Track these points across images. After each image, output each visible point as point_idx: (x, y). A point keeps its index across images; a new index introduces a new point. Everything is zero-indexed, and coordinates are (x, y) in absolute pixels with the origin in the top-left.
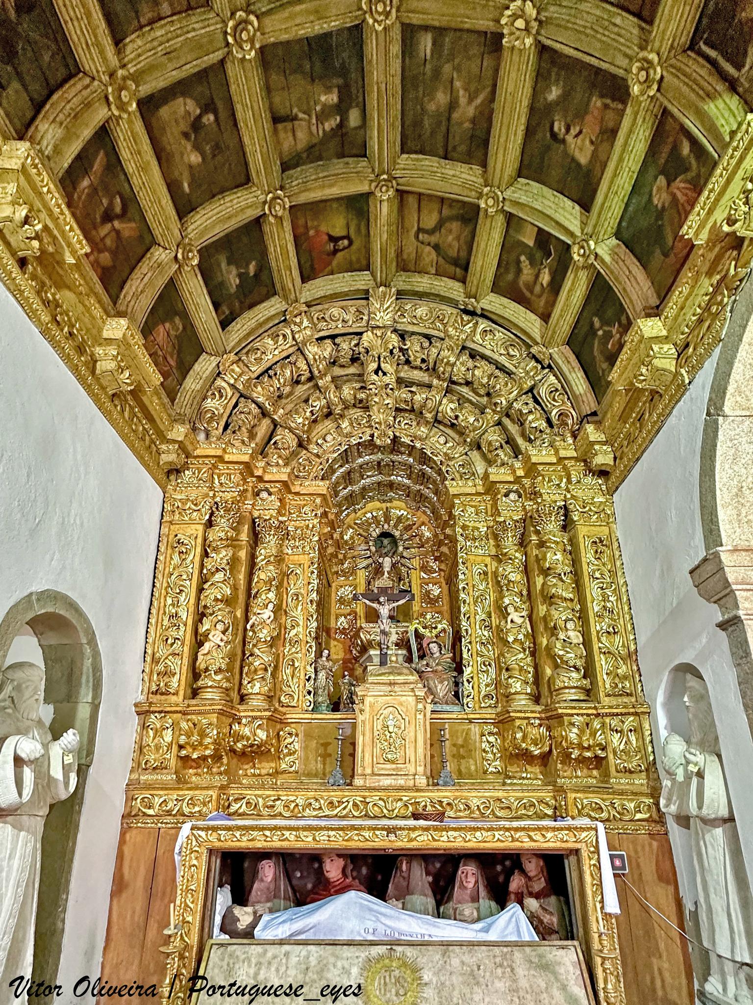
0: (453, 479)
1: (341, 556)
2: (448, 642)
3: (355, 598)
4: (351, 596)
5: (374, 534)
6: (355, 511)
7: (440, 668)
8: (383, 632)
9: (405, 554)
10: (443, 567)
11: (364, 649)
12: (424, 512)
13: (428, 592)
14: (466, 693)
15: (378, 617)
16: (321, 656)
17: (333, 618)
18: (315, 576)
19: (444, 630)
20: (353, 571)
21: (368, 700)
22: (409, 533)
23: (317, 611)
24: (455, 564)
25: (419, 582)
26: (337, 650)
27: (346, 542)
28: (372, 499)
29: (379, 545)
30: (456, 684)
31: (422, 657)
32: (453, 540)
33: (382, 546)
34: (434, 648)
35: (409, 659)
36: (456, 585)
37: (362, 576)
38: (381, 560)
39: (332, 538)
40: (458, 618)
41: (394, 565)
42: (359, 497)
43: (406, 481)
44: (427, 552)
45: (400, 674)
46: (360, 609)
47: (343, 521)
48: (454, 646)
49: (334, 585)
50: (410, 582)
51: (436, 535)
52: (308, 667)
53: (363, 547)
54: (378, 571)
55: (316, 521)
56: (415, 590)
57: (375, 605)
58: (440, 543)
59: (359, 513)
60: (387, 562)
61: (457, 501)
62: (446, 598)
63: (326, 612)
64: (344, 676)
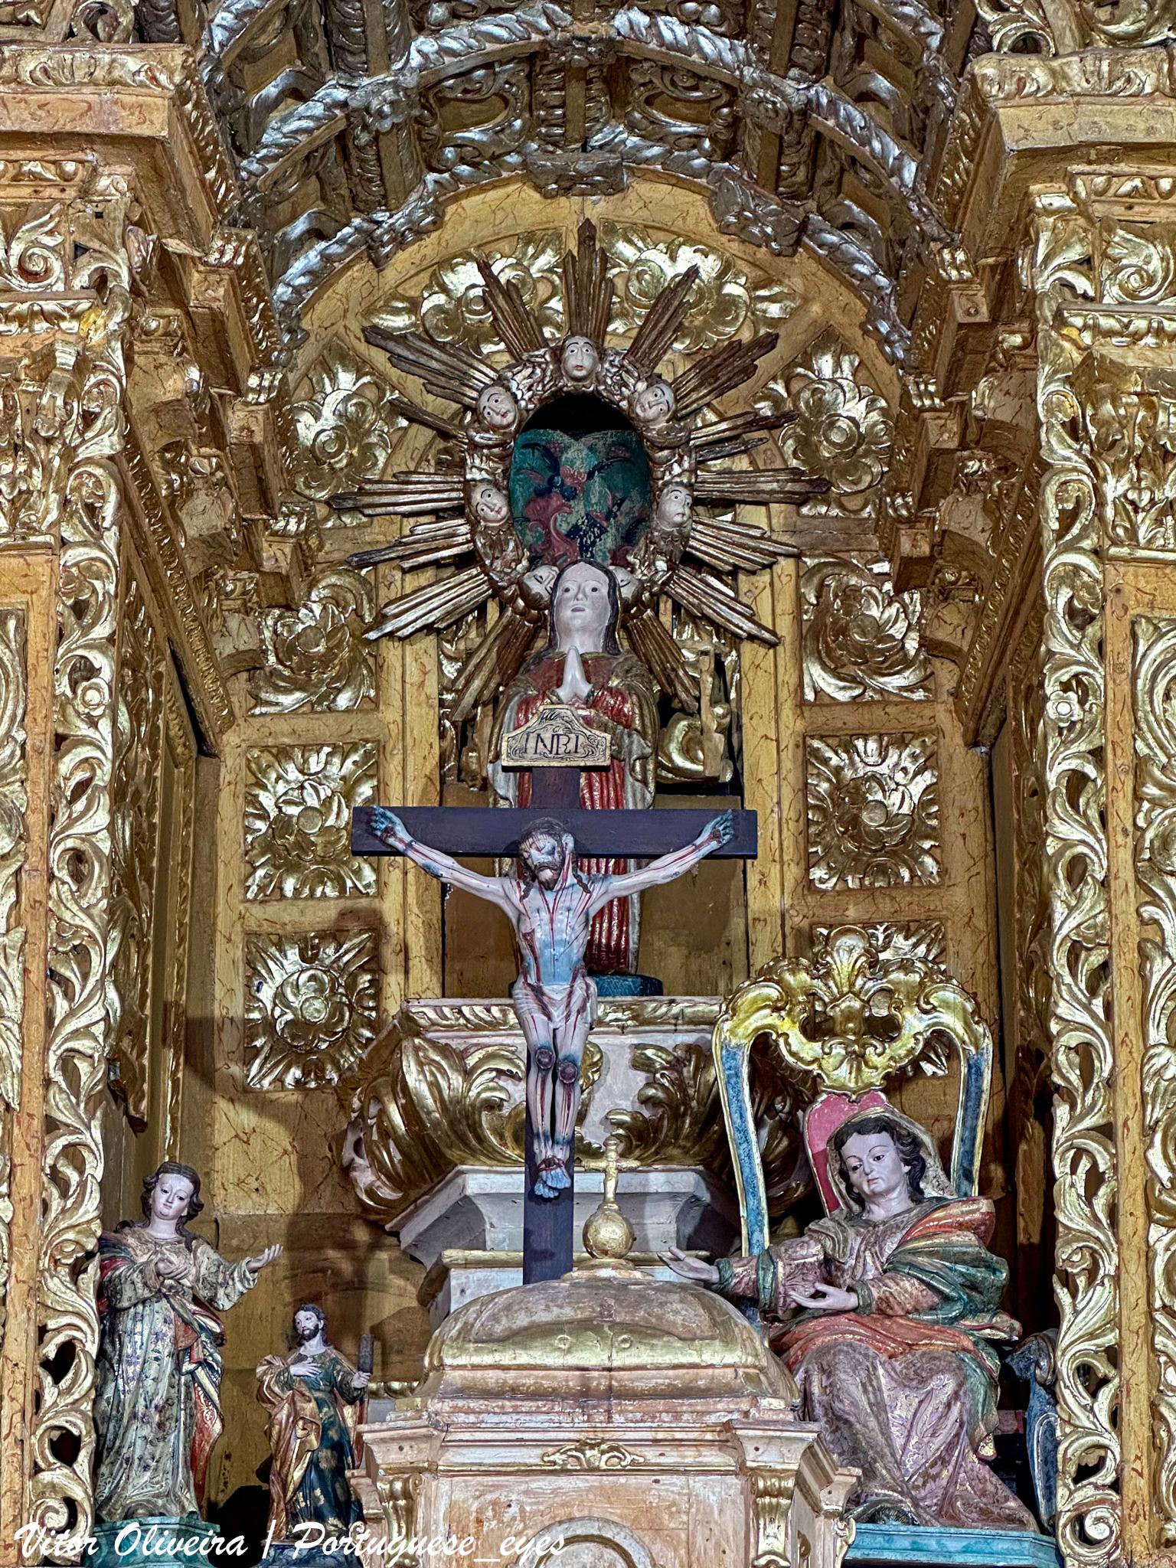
0: (1028, 45)
1: (275, 555)
2: (971, 1132)
3: (368, 837)
4: (340, 817)
5: (500, 410)
6: (371, 250)
7: (907, 1289)
8: (550, 1065)
9: (702, 544)
10: (951, 627)
11: (432, 1155)
12: (837, 264)
13: (851, 795)
14: (1071, 1450)
15: (521, 970)
16: (146, 1211)
17: (227, 957)
18: (97, 695)
19: (939, 1041)
20: (357, 654)
21: (441, 1497)
22: (735, 399)
23: (118, 915)
24: (1026, 617)
25: (792, 724)
26: (255, 1166)
27: (315, 456)
28: (486, 164)
29: (537, 488)
30: (1013, 1392)
31: (797, 1211)
32: (1019, 462)
33: (551, 485)
34: (876, 1161)
35: (714, 1230)
36: (1029, 754)
37: (416, 683)
38: (541, 580)
39: (217, 435)
40: (1036, 969)
41: (626, 619)
42: (399, 153)
43: (712, 45)
44: (852, 530)
45: (644, 1332)
46: (400, 895)
47: (291, 317)
48: (1004, 1143)
49: (231, 742)
50: (732, 729)
51: (905, 421)
52: (57, 1284)
53: (431, 489)
54: (524, 649)
55: (103, 326)
56: (771, 791)
57: (496, 888)
58: (935, 477)
59: (402, 262)
60: (582, 598)
61: (1050, 197)
62: (964, 828)
63: (178, 912)
64: (297, 1339)
